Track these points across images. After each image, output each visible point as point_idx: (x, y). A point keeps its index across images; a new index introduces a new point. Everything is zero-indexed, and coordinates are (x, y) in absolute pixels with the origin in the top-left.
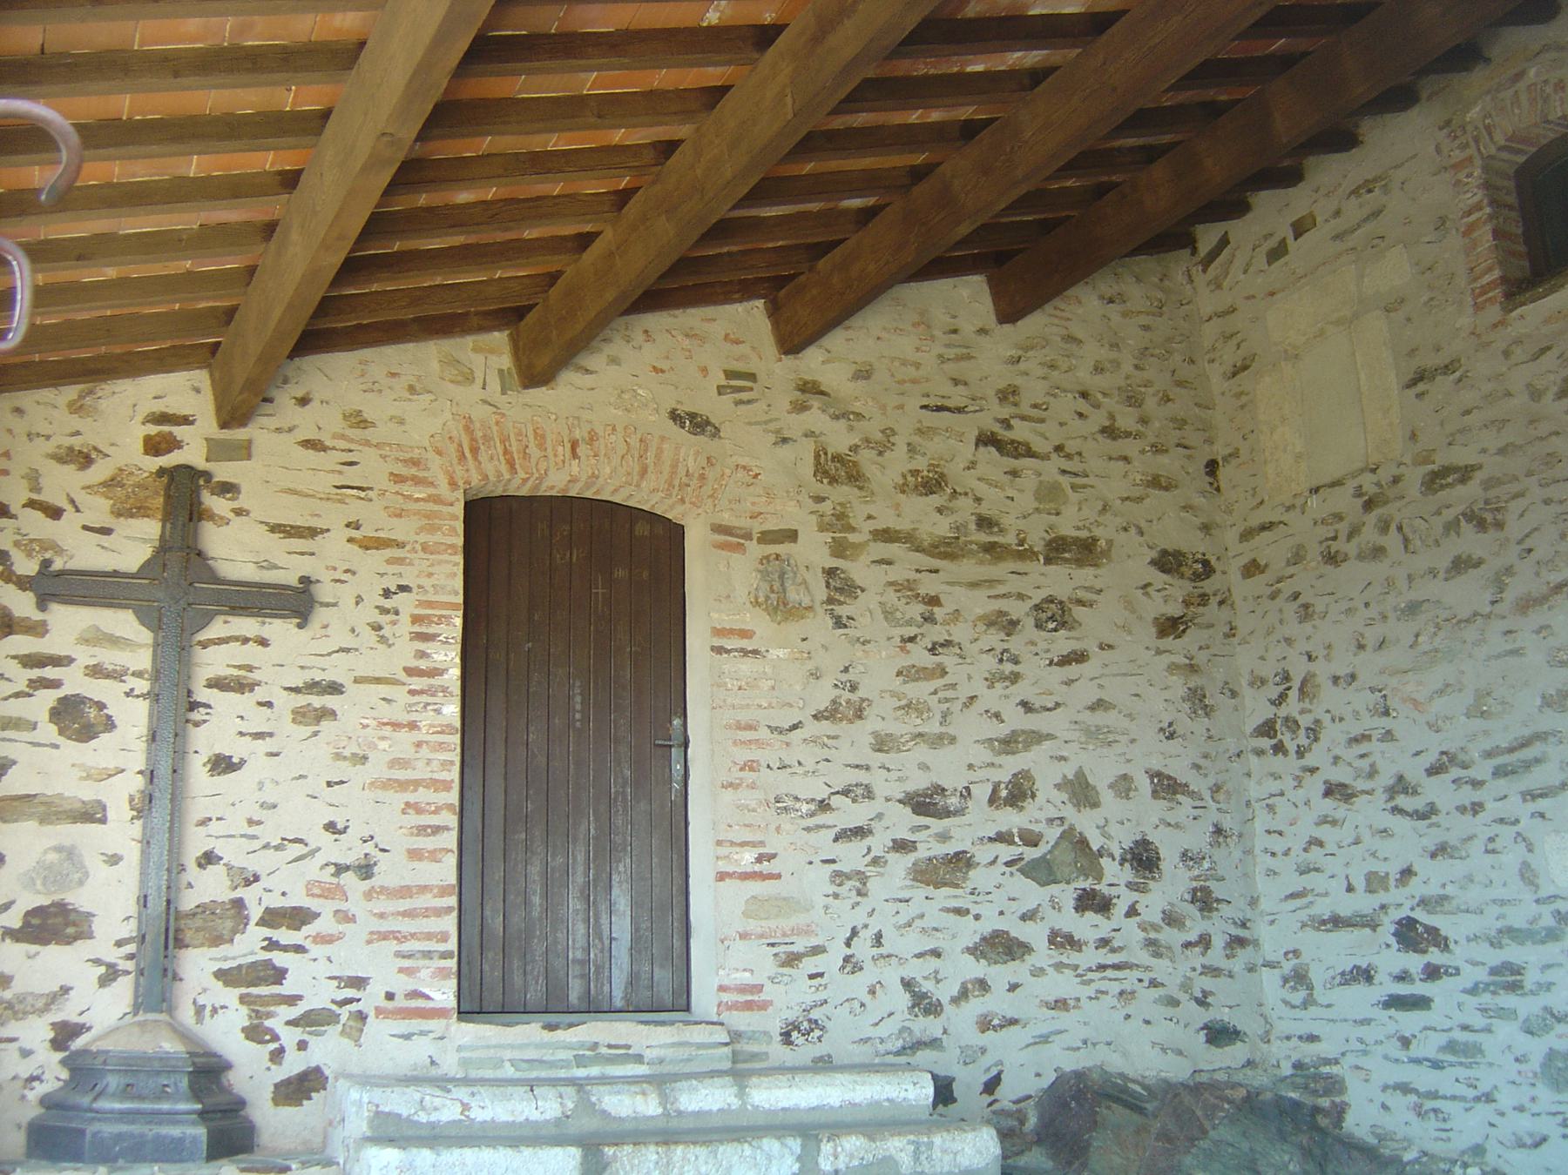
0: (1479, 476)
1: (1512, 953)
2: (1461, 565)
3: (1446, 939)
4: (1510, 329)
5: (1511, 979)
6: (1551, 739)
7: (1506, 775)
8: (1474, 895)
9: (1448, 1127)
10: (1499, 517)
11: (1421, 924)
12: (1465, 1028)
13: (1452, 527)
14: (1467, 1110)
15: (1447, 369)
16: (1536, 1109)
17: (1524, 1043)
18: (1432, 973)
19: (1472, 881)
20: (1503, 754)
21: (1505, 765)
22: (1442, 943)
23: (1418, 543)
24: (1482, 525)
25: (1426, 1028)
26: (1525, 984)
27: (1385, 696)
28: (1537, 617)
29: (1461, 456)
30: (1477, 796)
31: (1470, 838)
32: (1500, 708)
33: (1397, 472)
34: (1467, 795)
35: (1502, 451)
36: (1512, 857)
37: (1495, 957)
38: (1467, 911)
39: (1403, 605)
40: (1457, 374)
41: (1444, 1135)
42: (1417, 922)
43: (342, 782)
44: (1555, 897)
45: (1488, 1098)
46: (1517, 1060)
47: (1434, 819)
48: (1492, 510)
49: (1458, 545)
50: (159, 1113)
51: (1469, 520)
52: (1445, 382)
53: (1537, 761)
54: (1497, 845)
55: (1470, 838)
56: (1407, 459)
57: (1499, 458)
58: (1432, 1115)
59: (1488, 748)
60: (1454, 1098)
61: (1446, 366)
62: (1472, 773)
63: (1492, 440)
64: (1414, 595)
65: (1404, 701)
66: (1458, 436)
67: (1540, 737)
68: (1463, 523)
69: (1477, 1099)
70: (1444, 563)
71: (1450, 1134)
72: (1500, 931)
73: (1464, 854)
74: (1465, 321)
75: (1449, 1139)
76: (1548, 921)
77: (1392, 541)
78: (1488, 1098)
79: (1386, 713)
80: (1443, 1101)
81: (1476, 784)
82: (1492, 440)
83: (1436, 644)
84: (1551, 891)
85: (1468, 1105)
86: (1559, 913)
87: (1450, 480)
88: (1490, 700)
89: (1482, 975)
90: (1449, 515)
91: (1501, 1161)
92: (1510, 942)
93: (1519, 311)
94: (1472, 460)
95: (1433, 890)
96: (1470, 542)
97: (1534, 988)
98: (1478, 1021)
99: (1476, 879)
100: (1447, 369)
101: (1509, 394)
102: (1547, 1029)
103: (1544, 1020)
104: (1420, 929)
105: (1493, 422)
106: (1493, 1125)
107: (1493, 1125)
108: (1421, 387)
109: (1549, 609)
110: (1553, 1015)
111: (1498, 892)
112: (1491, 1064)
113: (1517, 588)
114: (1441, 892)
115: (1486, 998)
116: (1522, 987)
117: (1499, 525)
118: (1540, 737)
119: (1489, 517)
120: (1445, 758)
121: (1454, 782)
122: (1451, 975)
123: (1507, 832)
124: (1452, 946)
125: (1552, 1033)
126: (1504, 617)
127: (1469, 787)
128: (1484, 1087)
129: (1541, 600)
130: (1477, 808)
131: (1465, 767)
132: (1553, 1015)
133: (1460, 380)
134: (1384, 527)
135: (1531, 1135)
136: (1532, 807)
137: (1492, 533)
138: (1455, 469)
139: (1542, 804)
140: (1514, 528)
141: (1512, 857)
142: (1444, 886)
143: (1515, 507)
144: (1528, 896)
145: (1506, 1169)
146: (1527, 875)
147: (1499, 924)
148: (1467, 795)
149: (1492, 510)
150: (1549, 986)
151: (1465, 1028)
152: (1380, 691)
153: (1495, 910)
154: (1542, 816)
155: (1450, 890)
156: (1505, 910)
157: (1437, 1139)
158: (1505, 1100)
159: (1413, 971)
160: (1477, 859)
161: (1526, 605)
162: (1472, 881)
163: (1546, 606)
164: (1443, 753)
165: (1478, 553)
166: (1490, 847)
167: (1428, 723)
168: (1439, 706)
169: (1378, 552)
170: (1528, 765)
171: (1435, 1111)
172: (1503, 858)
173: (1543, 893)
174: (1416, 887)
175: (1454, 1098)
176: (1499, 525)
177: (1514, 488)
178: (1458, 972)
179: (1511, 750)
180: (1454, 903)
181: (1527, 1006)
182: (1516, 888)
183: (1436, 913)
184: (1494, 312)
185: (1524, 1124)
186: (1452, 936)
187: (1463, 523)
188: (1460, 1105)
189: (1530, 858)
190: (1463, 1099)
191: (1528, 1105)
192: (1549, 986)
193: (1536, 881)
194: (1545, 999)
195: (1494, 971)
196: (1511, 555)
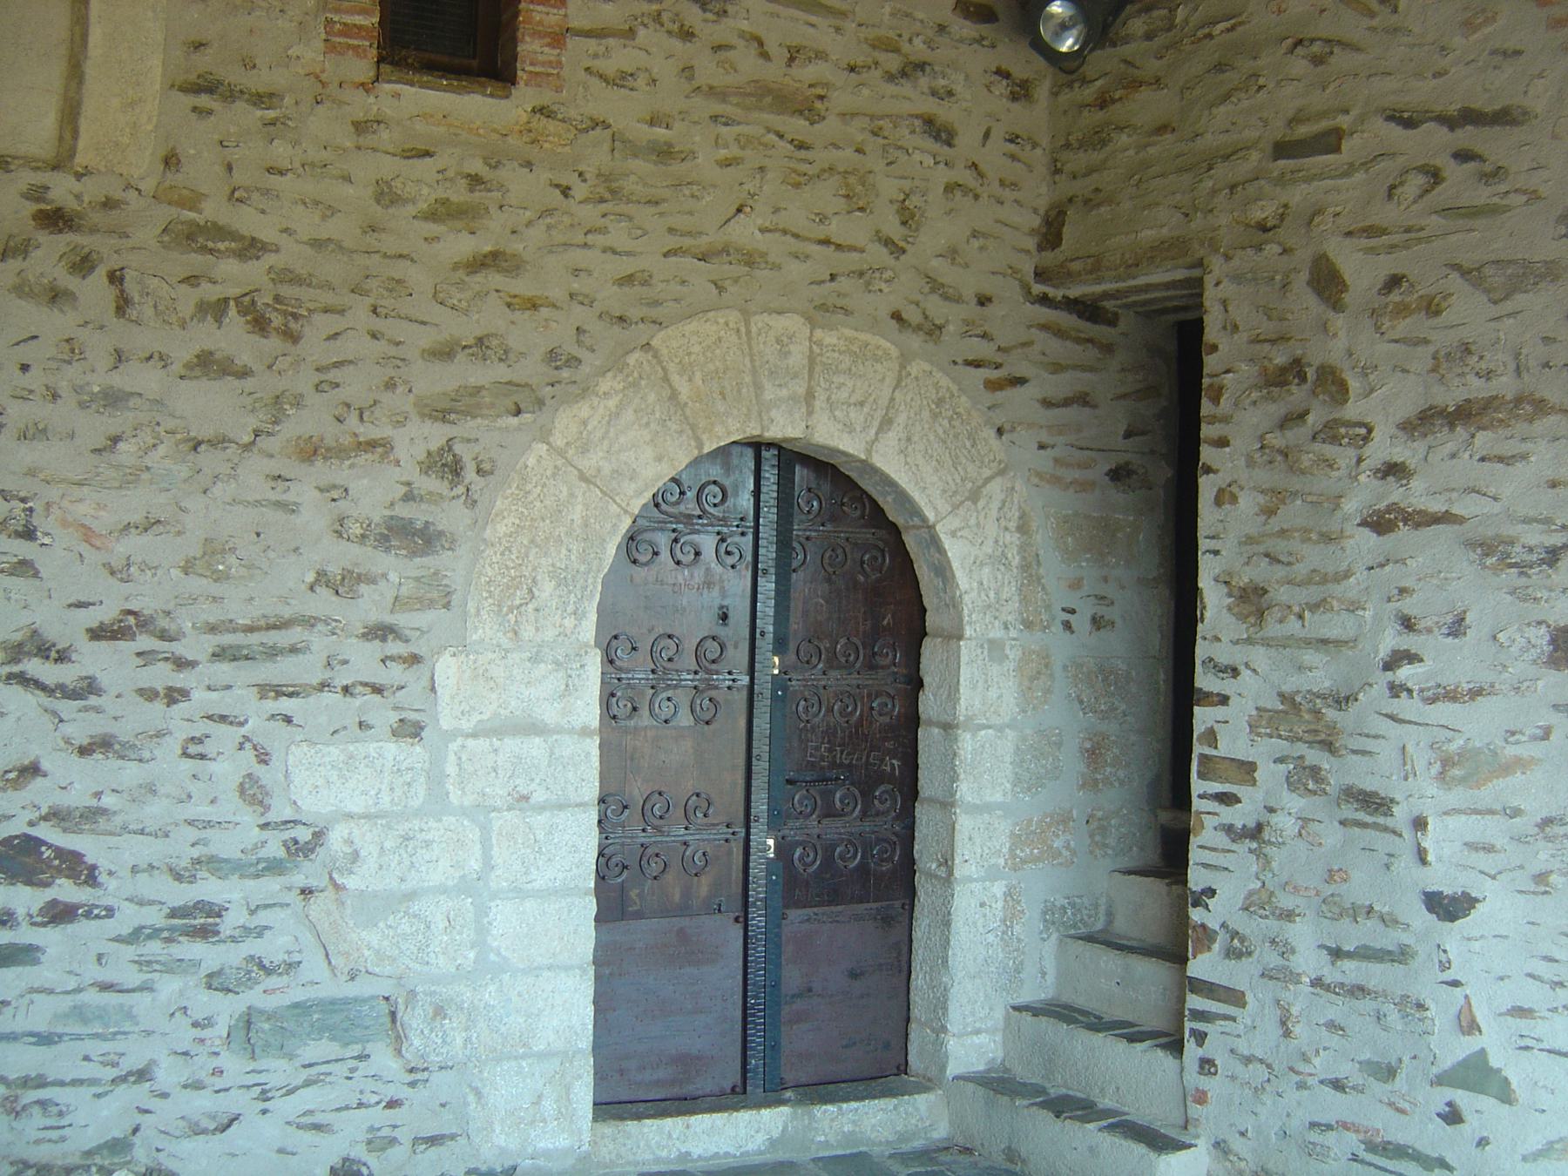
0: (270, 259)
1: (209, 889)
2: (207, 365)
3: (93, 868)
4: (372, 99)
5: (200, 921)
6: (320, 627)
7: (235, 659)
8: (155, 811)
9: (63, 1122)
10: (292, 325)
11: (50, 846)
12: (106, 987)
13: (216, 310)
14: (98, 1096)
15: (261, 99)
16: (219, 1083)
17: (204, 1002)
18: (60, 914)
19: (154, 792)
20: (234, 631)
21: (240, 647)
22: (88, 875)
23: (149, 312)
24: (260, 324)
25: (33, 990)
26: (221, 928)
27: (31, 510)
28: (322, 471)
29: (247, 221)
30: (181, 679)
31: (159, 734)
32: (243, 571)
33: (118, 194)
34: (161, 676)
35: (317, 244)
36: (228, 768)
37: (184, 894)
38: (142, 832)
39: (96, 389)
40: (271, 114)
41: (54, 1134)
42: (44, 843)
43: (17, 344)
44: (294, 822)
45: (142, 1075)
46: (195, 1025)
47: (93, 700)
48: (285, 313)
49: (207, 337)
50: (183, 916)
51: (243, 312)
52: (248, 116)
53: (294, 650)
54: (209, 748)
55: (159, 734)
56: (148, 185)
57: (309, 251)
58: (36, 1110)
59: (212, 620)
60: (77, 1082)
61: (260, 96)
62: (178, 648)
63: (307, 223)
64: (118, 380)
65: (65, 524)
66: (255, 196)
67: (310, 622)
68: (232, 311)
69: (123, 1079)
70: (184, 353)
71: (66, 1132)
72: (197, 862)
73: (146, 755)
74: (311, 53)
75: (63, 1139)
76: (275, 849)
77: (94, 290)
78: (142, 1075)
79: (28, 534)
80: (57, 1089)
81: (181, 664)
82: (307, 223)
83: (148, 461)
84: (288, 813)
85: (100, 1090)
86: (296, 842)
87: (221, 246)
88: (232, 560)
89: (154, 917)
90: (211, 292)
91: (161, 1155)
92: (207, 875)
93: (398, 87)
94: (267, 234)
95: (78, 798)
96: (233, 338)
97: (237, 933)
98: (133, 977)
99: (162, 790)
100: (261, 99)
101: (347, 179)
102: (249, 981)
103: (249, 972)
104: (47, 853)
105: (317, 203)
106: (147, 1111)
107: (147, 1111)
108: (204, 100)
109: (351, 466)
110: (262, 966)
111: (202, 810)
112: (148, 1033)
113: (298, 425)
114: (94, 803)
115: (154, 948)
116: (218, 933)
117: (293, 337)
118: (310, 622)
119: (277, 320)
120: (131, 620)
121: (139, 654)
122: (98, 917)
123: (225, 737)
124: (103, 878)
125: (259, 988)
126: (272, 456)
127: (169, 666)
128: (131, 1063)
129: (338, 453)
130: (174, 696)
131: (164, 636)
132: (262, 966)
133: (273, 123)
134: (83, 264)
135: (213, 1117)
136: (271, 706)
137: (274, 343)
138: (233, 236)
139: (285, 705)
140: (314, 346)
141: (228, 768)
142: (98, 795)
143: (325, 324)
144: (248, 818)
145: (170, 1164)
146: (252, 793)
147: (195, 853)
148: (161, 676)
149: (285, 313)
150: (260, 931)
151: (106, 987)
152: (23, 500)
153: (192, 834)
154: (288, 720)
155: (108, 801)
156: (209, 833)
157: (38, 1142)
158: (168, 1074)
159: (21, 912)
160: (167, 762)
161: (310, 451)
162: (154, 792)
163: (347, 463)
164: (130, 612)
165: (244, 358)
166: (193, 749)
167: (107, 565)
168: (132, 545)
169: (56, 296)
170: (273, 653)
171: (42, 1104)
172: (213, 767)
173: (272, 817)
174: (40, 793)
175: (77, 1082)
176: (293, 337)
177: (327, 298)
178: (110, 912)
179: (250, 629)
180: (118, 820)
181: (208, 955)
182: (231, 806)
183: (81, 832)
184: (362, 68)
185: (202, 1103)
186: (104, 863)
187: (232, 311)
188: (86, 1092)
189: (260, 770)
190: (93, 1082)
191: (209, 1080)
192: (260, 931)
193: (267, 801)
194: (252, 947)
195: (174, 913)
196: (304, 382)
